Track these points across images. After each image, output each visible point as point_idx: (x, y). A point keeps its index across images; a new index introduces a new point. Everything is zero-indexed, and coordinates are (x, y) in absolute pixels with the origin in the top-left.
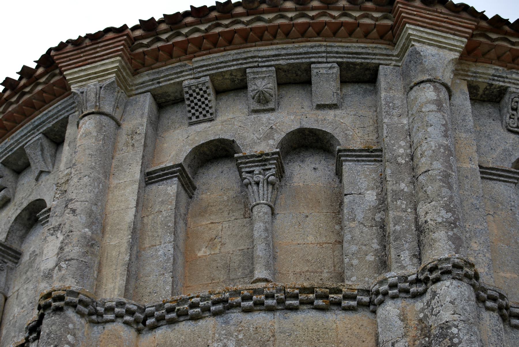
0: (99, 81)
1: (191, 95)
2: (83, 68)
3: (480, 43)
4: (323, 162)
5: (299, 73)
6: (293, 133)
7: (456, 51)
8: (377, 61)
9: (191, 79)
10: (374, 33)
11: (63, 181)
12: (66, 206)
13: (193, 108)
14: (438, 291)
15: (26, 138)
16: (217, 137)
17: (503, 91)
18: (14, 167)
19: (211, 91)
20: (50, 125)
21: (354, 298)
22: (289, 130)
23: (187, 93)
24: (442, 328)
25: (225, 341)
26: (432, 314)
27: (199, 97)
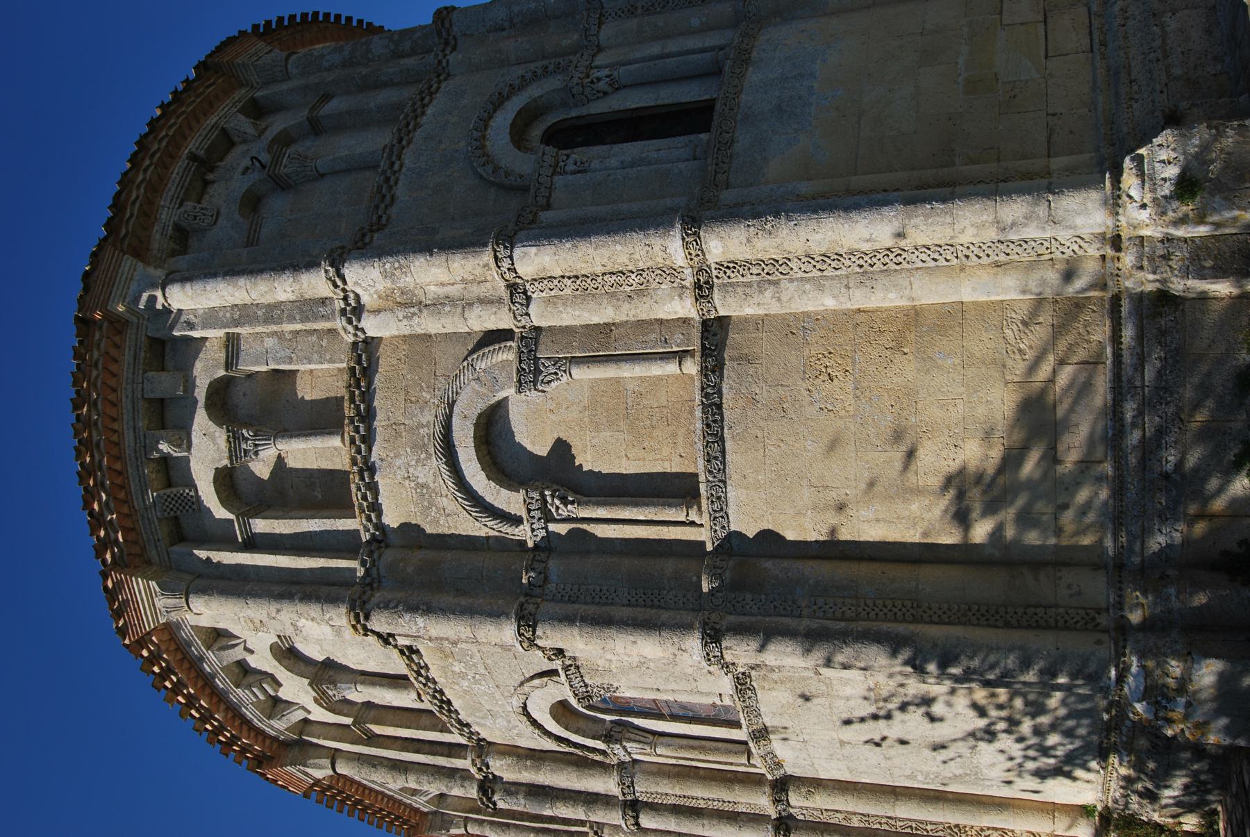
0: (156, 596)
1: (172, 509)
2: (143, 612)
4: (238, 388)
5: (152, 409)
6: (209, 415)
7: (136, 265)
8: (143, 338)
9: (155, 510)
10: (117, 339)
11: (252, 626)
12: (274, 618)
13: (184, 508)
14: (354, 280)
15: (213, 665)
16: (212, 484)
17: (177, 227)
18: (241, 676)
19: (168, 491)
21: (360, 356)
22: (207, 418)
23: (169, 513)
24: (386, 277)
25: (396, 468)
26: (374, 287)
27: (174, 502)
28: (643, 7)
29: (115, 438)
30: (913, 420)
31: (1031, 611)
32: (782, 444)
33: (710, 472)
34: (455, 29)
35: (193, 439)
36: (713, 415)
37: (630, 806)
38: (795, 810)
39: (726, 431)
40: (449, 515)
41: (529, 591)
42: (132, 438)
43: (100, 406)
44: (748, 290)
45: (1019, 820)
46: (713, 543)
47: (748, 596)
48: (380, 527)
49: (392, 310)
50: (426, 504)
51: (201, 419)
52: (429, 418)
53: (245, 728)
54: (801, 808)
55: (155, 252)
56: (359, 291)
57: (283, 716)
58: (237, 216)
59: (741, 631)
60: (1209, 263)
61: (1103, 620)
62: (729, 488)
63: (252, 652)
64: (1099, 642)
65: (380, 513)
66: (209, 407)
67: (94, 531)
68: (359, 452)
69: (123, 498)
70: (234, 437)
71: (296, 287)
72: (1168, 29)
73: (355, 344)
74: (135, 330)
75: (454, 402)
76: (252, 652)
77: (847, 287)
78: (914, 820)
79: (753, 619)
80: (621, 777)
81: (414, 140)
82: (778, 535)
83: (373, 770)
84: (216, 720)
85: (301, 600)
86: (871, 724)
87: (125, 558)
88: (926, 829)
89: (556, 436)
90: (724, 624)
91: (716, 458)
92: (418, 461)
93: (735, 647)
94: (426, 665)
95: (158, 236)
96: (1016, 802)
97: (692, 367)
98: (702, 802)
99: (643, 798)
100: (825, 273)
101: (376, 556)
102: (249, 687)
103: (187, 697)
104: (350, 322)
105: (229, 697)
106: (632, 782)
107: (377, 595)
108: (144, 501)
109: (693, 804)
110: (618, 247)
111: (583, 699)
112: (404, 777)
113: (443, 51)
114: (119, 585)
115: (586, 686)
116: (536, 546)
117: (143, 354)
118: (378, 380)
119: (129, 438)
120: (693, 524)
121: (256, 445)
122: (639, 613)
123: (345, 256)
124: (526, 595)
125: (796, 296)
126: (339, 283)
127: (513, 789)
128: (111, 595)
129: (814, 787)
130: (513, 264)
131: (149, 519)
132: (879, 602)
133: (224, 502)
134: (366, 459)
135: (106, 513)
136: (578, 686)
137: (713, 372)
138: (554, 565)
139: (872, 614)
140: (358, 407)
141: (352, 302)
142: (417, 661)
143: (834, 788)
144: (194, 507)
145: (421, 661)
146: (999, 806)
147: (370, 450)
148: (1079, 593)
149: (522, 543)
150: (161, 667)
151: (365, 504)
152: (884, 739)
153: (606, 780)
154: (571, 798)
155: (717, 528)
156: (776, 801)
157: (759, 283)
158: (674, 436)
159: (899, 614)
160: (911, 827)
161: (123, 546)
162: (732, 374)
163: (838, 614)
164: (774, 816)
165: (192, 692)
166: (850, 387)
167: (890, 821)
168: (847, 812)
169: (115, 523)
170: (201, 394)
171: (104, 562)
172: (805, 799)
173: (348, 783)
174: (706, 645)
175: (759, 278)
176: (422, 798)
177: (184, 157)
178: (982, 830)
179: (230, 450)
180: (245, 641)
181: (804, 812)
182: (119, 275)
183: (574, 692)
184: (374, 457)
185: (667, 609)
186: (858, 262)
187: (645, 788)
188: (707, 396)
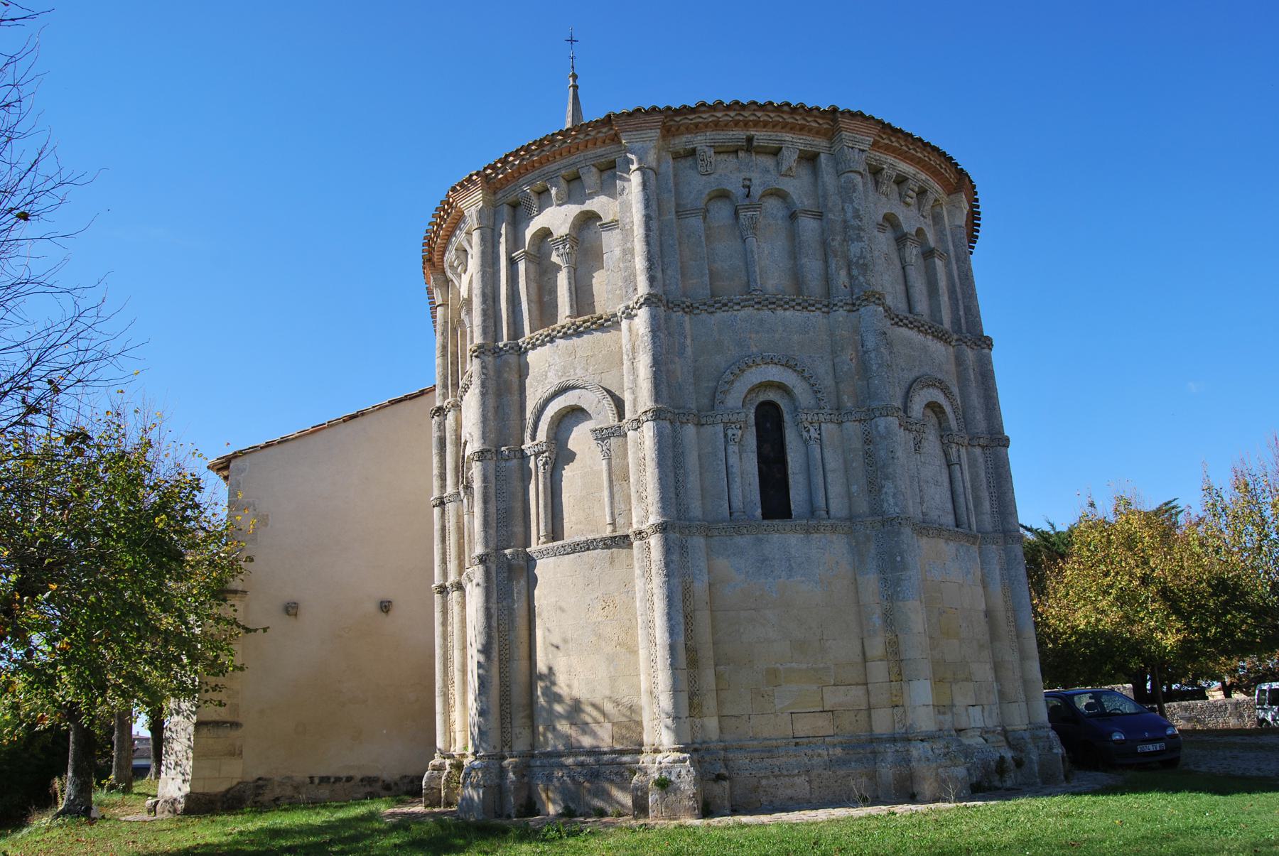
3: (671, 126)
8: (613, 157)
21: (609, 320)
28: (869, 449)
31: (508, 715)
35: (564, 207)
41: (498, 452)
42: (554, 169)
47: (505, 575)
48: (526, 351)
49: (630, 340)
51: (573, 210)
55: (673, 142)
58: (707, 192)
59: (487, 574)
60: (639, 793)
61: (506, 749)
64: (495, 747)
66: (583, 213)
68: (559, 332)
69: (521, 171)
72: (796, 778)
74: (616, 150)
79: (494, 579)
81: (761, 311)
85: (483, 310)
90: (489, 564)
92: (557, 370)
95: (684, 139)
97: (608, 532)
101: (511, 351)
102: (458, 257)
107: (490, 359)
108: (524, 184)
109: (447, 538)
113: (846, 304)
114: (475, 183)
116: (523, 450)
118: (597, 334)
119: (554, 167)
120: (539, 539)
122: (493, 517)
123: (654, 305)
124: (497, 451)
132: (507, 642)
133: (534, 236)
137: (604, 544)
138: (515, 462)
139: (501, 639)
140: (581, 326)
147: (561, 338)
148: (517, 738)
149: (523, 443)
154: (442, 464)
163: (500, 622)
164: (447, 584)
166: (600, 619)
177: (748, 133)
182: (645, 132)
185: (497, 532)
187: (450, 507)
188: (592, 542)
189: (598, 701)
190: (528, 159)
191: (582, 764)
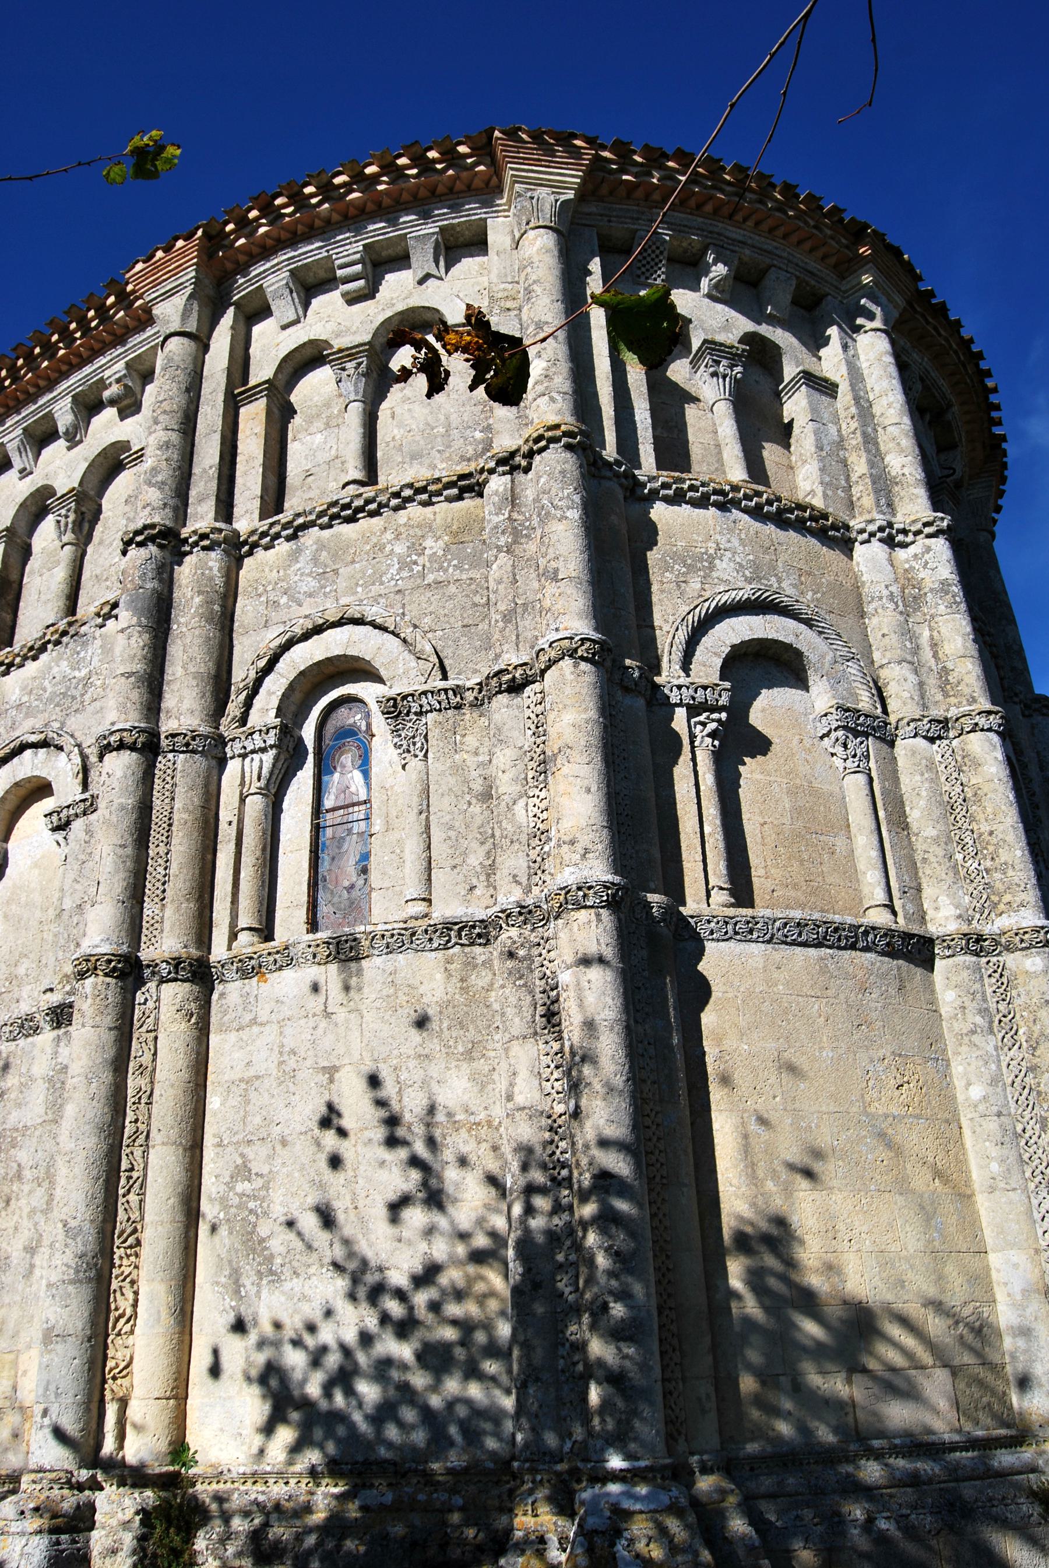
10: (832, 261)
20: (457, 221)
21: (838, 530)
29: (739, 217)
30: (872, 1187)
32: (822, 1019)
33: (786, 924)
34: (1040, 718)
36: (847, 938)
37: (152, 742)
38: (153, 990)
39: (828, 951)
40: (679, 587)
42: (734, 236)
43: (778, 214)
44: (979, 996)
45: (162, 1341)
46: (692, 917)
47: (644, 953)
50: (689, 562)
51: (744, 325)
52: (787, 590)
53: (284, 235)
54: (158, 1000)
56: (912, 549)
57: (291, 292)
62: (762, 946)
63: (421, 282)
65: (669, 501)
67: (647, 151)
70: (736, 355)
71: (911, 480)
73: (847, 528)
75: (811, 626)
76: (421, 282)
77: (999, 1114)
78: (145, 1175)
80: (206, 737)
82: (706, 1002)
83: (183, 387)
84: (320, 203)
86: (373, 1115)
87: (602, 174)
88: (129, 1191)
89: (774, 740)
91: (800, 935)
93: (601, 926)
94: (433, 504)
96: (187, 1337)
98: (162, 849)
99: (161, 763)
100: (1009, 1089)
103: (375, 179)
104: (881, 529)
105: (349, 231)
106: (194, 752)
110: (1019, 853)
111: (395, 706)
112: (176, 427)
114: (575, 153)
115: (420, 714)
116: (657, 687)
117: (813, 283)
119: (735, 233)
121: (724, 377)
125: (979, 1053)
126: (928, 530)
127: (165, 576)
128: (565, 139)
129: (197, 1023)
130: (982, 730)
131: (638, 219)
134: (736, 503)
135: (663, 173)
136: (424, 701)
137: (888, 944)
141: (900, 538)
142: (445, 493)
143: (198, 1053)
144: (643, 279)
145: (442, 498)
146: (182, 1309)
147: (745, 511)
150: (434, 161)
151: (686, 486)
152: (342, 1133)
153: (197, 713)
154: (155, 656)
155: (713, 925)
156: (177, 963)
157: (987, 1009)
158: (796, 886)
159: (654, 1158)
160: (132, 1169)
161: (617, 176)
162: (885, 967)
165: (381, 188)
167: (143, 1137)
168: (154, 1070)
169: (646, 179)
170: (765, 330)
171: (604, 148)
172: (177, 1007)
173: (97, 346)
174: (605, 887)
175: (993, 1011)
176: (16, 442)
178: (133, 1282)
179: (721, 345)
180: (441, 279)
181: (150, 1004)
183: (413, 695)
184: (736, 513)
186: (1029, 1127)
189: (914, 1310)
190: (706, 187)
191: (914, 1480)
